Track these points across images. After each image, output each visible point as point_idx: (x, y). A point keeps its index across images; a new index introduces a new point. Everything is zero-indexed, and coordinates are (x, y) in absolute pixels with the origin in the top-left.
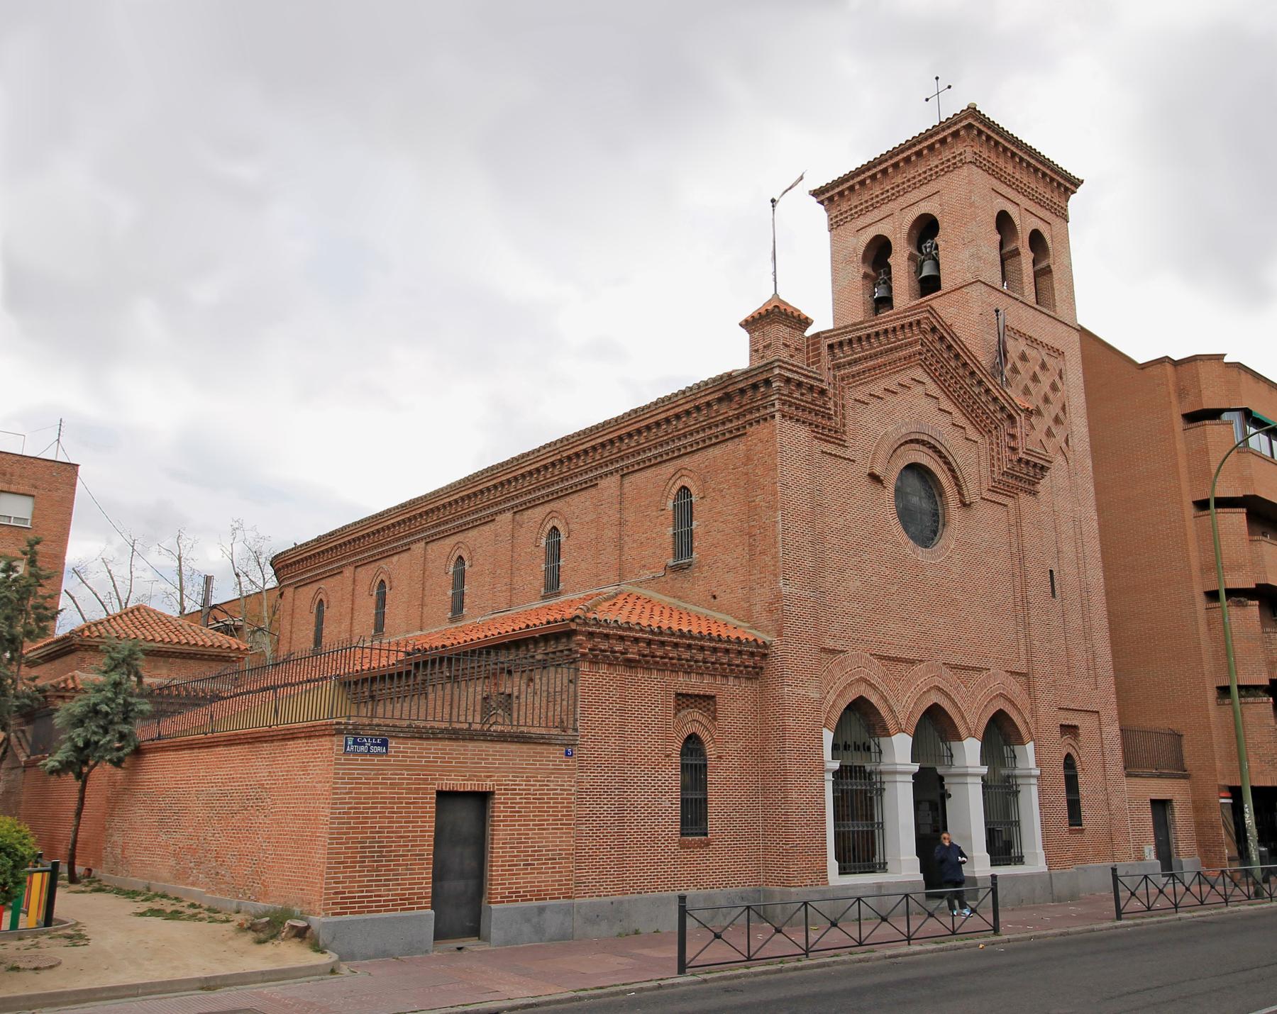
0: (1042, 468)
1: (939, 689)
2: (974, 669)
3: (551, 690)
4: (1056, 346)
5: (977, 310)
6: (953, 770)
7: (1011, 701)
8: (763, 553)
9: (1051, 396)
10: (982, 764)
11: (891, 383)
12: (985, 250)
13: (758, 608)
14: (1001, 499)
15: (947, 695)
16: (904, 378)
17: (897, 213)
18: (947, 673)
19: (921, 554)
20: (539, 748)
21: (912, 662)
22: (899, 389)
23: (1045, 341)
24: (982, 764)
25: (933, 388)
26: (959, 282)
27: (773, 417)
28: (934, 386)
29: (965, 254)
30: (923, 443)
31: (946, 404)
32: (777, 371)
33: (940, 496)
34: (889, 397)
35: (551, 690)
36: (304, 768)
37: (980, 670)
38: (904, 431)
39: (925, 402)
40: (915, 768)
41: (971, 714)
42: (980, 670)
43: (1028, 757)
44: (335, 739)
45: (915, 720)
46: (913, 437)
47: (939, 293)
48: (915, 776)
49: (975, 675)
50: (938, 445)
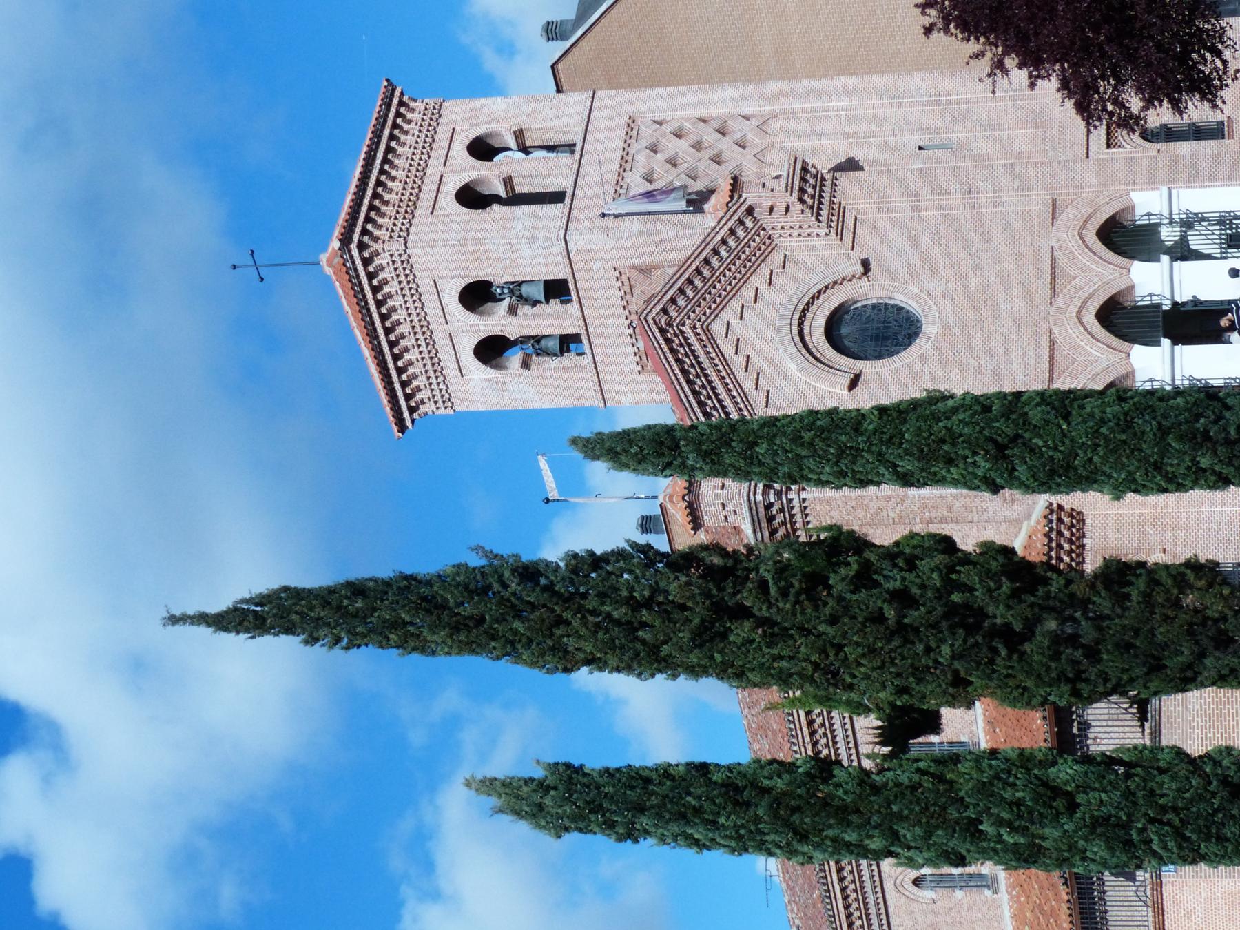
0: (805, 169)
1: (1079, 312)
2: (1053, 268)
3: (1106, 717)
4: (623, 127)
5: (602, 239)
6: (1168, 295)
7: (1086, 221)
8: (950, 509)
9: (693, 138)
10: (1158, 260)
11: (737, 364)
12: (520, 227)
13: (1007, 513)
14: (849, 224)
15: (1085, 302)
16: (727, 347)
17: (449, 329)
18: (1060, 301)
19: (930, 328)
20: (1163, 719)
21: (1052, 343)
22: (741, 352)
23: (621, 145)
24: (1158, 260)
25: (730, 313)
26: (561, 259)
27: (804, 500)
28: (728, 309)
29: (527, 252)
30: (801, 324)
31: (746, 295)
32: (759, 498)
33: (856, 302)
34: (753, 366)
35: (1106, 717)
36: (1189, 913)
37: (1053, 259)
38: (793, 349)
39: (749, 320)
40: (1166, 342)
41: (1104, 274)
42: (1053, 259)
43: (1148, 203)
44: (1164, 880)
45: (1116, 342)
46: (797, 338)
47: (571, 282)
48: (1175, 342)
49: (1060, 264)
50: (801, 307)
